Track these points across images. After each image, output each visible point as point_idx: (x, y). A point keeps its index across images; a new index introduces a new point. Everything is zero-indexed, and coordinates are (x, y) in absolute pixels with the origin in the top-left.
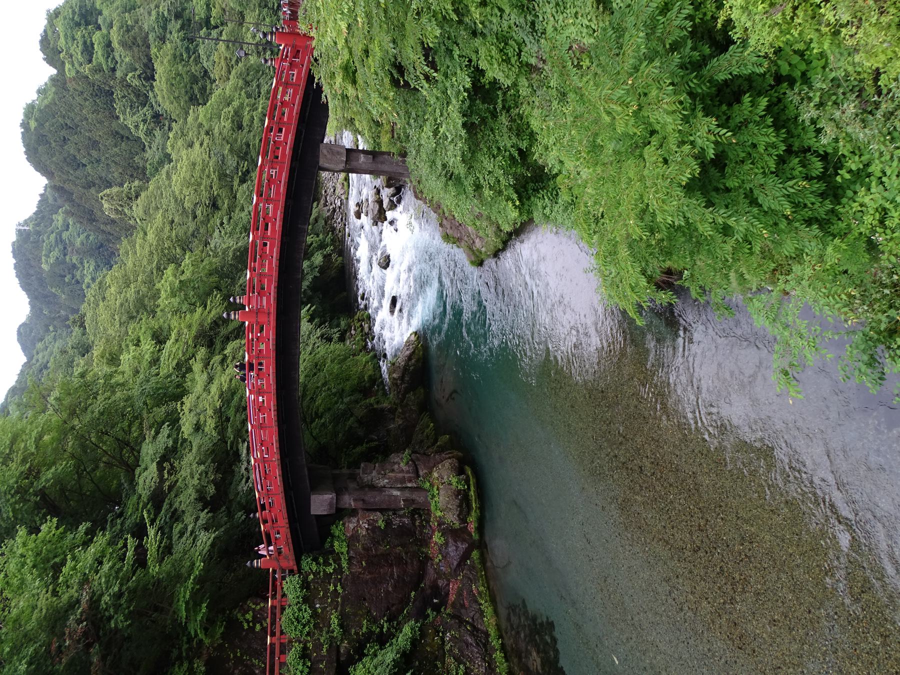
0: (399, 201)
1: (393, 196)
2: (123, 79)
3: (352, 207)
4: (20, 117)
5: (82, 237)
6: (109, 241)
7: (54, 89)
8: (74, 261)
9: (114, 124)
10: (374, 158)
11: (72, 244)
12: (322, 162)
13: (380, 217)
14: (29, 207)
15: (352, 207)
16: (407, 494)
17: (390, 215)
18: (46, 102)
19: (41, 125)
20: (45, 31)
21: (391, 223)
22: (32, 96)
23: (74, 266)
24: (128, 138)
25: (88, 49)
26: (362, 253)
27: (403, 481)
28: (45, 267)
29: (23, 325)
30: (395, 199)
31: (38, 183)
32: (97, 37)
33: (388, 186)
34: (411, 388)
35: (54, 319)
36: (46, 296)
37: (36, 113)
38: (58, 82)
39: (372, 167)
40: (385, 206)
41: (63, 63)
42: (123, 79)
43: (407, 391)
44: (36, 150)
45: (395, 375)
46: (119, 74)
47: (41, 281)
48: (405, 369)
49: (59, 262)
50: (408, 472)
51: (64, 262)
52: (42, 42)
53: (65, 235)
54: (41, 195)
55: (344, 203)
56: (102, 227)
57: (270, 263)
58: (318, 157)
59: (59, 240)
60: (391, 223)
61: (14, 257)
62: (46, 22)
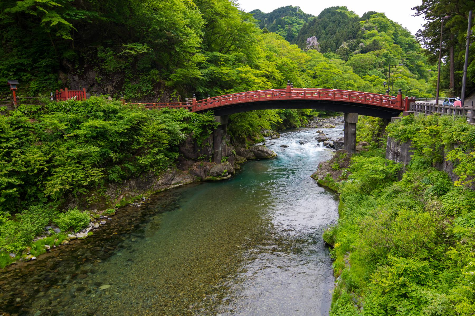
0: (327, 147)
1: (330, 145)
2: (361, 42)
3: (321, 130)
4: (341, 5)
5: (295, 30)
6: (295, 40)
7: (353, 17)
8: (286, 28)
9: (342, 40)
10: (353, 134)
11: (292, 27)
12: (350, 114)
13: (319, 140)
14: (306, 10)
15: (321, 130)
16: (220, 152)
17: (321, 143)
18: (348, 15)
19: (340, 13)
20: (376, 13)
21: (318, 145)
22: (350, 9)
23: (284, 28)
24: (337, 44)
25: (370, 28)
26: (304, 134)
27: (225, 150)
28: (283, 18)
29: (260, 11)
30: (328, 145)
31: (316, 13)
32: (375, 31)
33: (334, 143)
34: (255, 154)
35: (263, 22)
36: (272, 19)
37: (343, 11)
38: (356, 19)
39: (349, 133)
40: (325, 142)
41: (365, 20)
42: (361, 42)
43: (254, 152)
44: (329, 12)
45: (260, 147)
46: (362, 40)
47: (278, 17)
48: (263, 152)
49: (286, 23)
50: (228, 153)
51: (285, 24)
52: (372, 12)
53: (296, 24)
54: (311, 15)
55: (320, 127)
56: (301, 37)
57: (324, 97)
58: (352, 113)
59: (294, 22)
60: (318, 145)
61: (286, 7)
62: (380, 13)
